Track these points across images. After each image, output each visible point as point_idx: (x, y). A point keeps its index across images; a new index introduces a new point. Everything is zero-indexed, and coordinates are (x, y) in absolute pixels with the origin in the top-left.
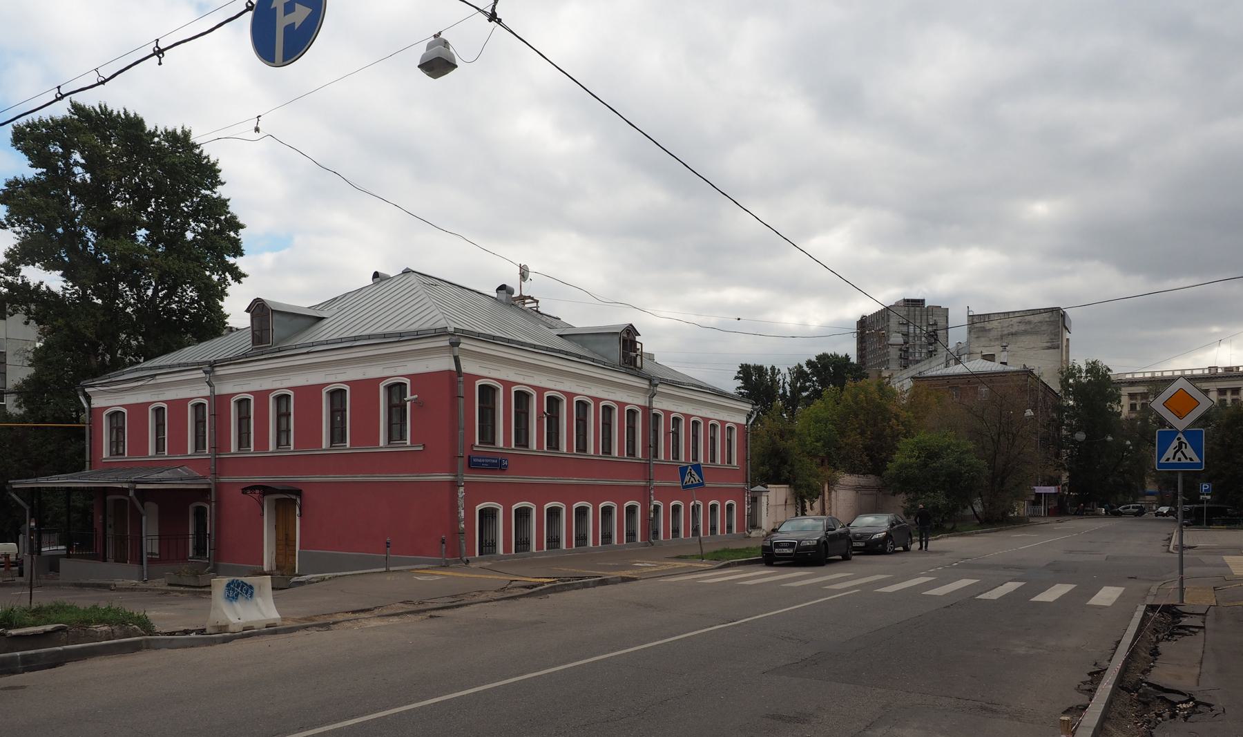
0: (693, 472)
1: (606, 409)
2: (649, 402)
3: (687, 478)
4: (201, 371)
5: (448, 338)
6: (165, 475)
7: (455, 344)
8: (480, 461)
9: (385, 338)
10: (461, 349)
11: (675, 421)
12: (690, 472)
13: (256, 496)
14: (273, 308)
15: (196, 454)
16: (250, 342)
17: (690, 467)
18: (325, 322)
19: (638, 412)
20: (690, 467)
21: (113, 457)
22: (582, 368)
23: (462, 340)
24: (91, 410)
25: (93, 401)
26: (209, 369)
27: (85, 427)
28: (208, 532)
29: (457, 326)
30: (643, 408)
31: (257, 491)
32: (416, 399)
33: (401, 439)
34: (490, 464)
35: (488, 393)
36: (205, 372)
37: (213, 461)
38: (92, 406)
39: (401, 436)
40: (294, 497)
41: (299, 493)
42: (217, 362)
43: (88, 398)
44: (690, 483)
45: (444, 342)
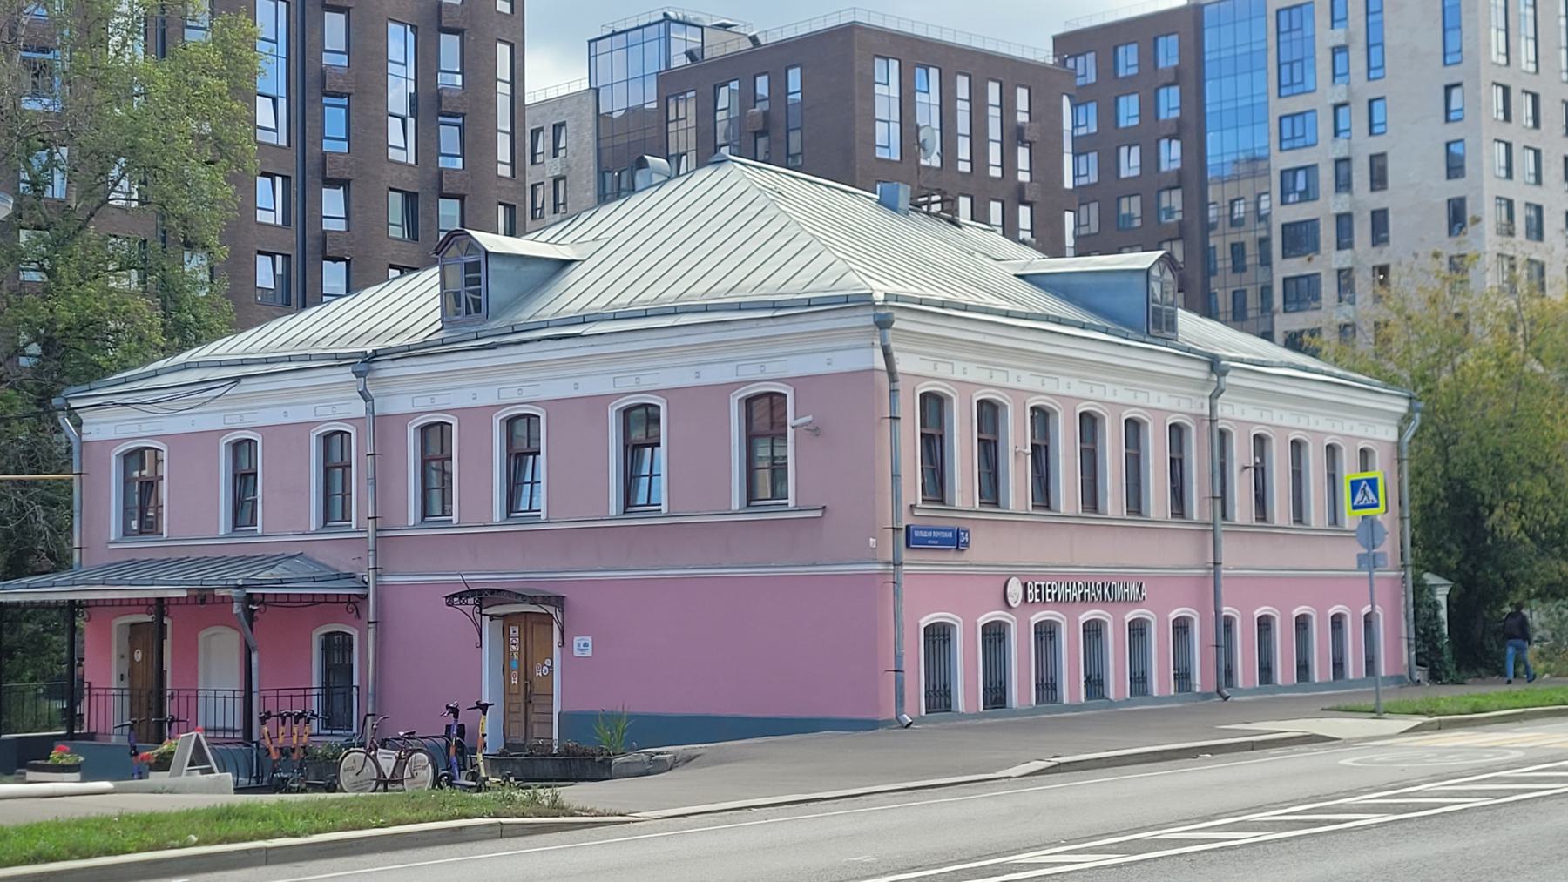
0: (1368, 489)
1: (985, 407)
2: (1211, 408)
3: (1359, 496)
4: (349, 369)
5: (871, 311)
6: (278, 572)
7: (883, 324)
8: (925, 535)
9: (740, 309)
10: (896, 329)
11: (1129, 424)
12: (1364, 489)
13: (468, 609)
14: (490, 250)
15: (325, 530)
16: (438, 314)
17: (1364, 483)
18: (574, 274)
19: (1189, 428)
20: (1364, 483)
21: (129, 539)
22: (1093, 349)
23: (897, 314)
24: (82, 443)
25: (84, 429)
26: (363, 368)
27: (72, 479)
28: (356, 682)
29: (889, 290)
30: (1198, 418)
31: (471, 601)
32: (810, 422)
33: (443, 514)
34: (942, 541)
35: (933, 405)
36: (358, 374)
37: (371, 539)
38: (84, 438)
39: (251, 521)
40: (551, 610)
41: (559, 601)
42: (379, 353)
43: (78, 424)
44: (1363, 503)
45: (865, 319)
